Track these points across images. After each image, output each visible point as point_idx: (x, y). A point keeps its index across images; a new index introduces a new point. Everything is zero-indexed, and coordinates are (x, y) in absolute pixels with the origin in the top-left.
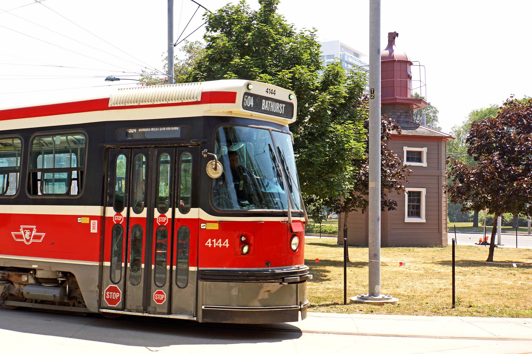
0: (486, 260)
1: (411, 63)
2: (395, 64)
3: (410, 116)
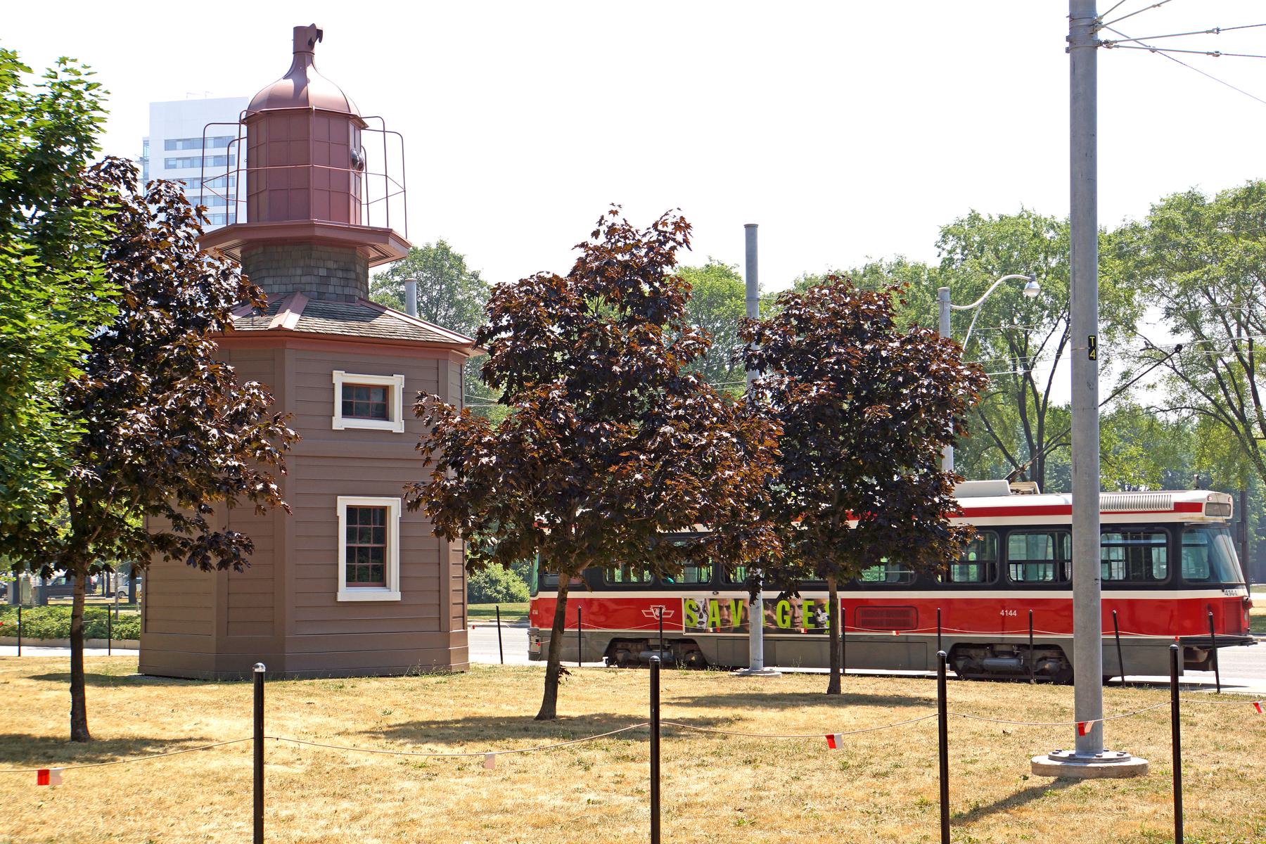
0: (536, 714)
1: (361, 124)
2: (313, 119)
3: (357, 280)
